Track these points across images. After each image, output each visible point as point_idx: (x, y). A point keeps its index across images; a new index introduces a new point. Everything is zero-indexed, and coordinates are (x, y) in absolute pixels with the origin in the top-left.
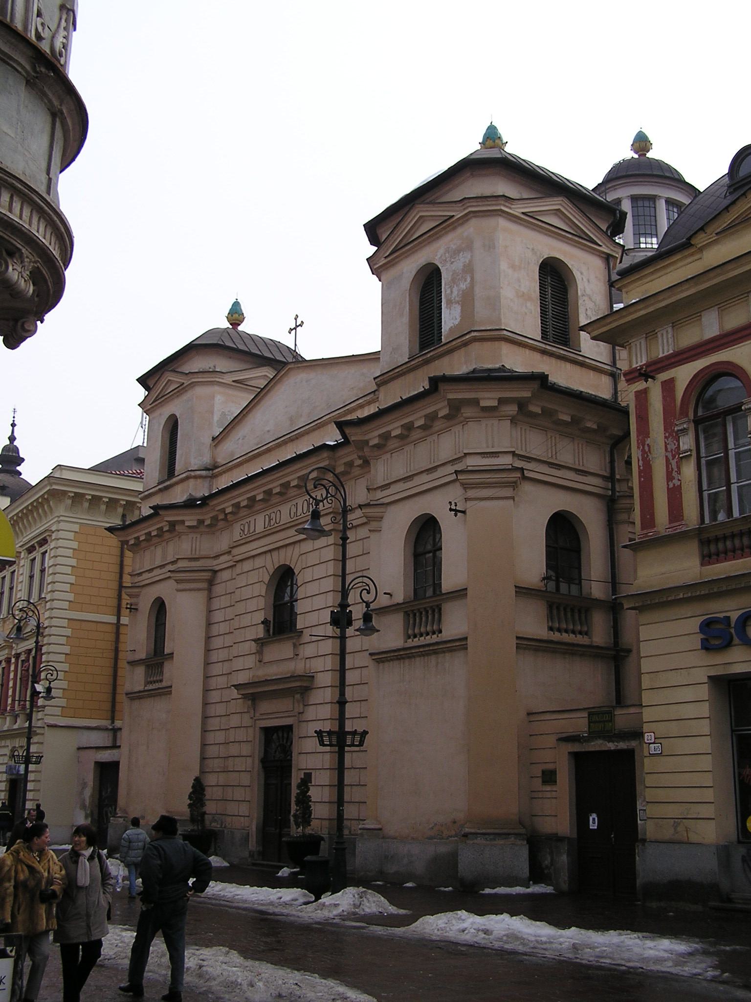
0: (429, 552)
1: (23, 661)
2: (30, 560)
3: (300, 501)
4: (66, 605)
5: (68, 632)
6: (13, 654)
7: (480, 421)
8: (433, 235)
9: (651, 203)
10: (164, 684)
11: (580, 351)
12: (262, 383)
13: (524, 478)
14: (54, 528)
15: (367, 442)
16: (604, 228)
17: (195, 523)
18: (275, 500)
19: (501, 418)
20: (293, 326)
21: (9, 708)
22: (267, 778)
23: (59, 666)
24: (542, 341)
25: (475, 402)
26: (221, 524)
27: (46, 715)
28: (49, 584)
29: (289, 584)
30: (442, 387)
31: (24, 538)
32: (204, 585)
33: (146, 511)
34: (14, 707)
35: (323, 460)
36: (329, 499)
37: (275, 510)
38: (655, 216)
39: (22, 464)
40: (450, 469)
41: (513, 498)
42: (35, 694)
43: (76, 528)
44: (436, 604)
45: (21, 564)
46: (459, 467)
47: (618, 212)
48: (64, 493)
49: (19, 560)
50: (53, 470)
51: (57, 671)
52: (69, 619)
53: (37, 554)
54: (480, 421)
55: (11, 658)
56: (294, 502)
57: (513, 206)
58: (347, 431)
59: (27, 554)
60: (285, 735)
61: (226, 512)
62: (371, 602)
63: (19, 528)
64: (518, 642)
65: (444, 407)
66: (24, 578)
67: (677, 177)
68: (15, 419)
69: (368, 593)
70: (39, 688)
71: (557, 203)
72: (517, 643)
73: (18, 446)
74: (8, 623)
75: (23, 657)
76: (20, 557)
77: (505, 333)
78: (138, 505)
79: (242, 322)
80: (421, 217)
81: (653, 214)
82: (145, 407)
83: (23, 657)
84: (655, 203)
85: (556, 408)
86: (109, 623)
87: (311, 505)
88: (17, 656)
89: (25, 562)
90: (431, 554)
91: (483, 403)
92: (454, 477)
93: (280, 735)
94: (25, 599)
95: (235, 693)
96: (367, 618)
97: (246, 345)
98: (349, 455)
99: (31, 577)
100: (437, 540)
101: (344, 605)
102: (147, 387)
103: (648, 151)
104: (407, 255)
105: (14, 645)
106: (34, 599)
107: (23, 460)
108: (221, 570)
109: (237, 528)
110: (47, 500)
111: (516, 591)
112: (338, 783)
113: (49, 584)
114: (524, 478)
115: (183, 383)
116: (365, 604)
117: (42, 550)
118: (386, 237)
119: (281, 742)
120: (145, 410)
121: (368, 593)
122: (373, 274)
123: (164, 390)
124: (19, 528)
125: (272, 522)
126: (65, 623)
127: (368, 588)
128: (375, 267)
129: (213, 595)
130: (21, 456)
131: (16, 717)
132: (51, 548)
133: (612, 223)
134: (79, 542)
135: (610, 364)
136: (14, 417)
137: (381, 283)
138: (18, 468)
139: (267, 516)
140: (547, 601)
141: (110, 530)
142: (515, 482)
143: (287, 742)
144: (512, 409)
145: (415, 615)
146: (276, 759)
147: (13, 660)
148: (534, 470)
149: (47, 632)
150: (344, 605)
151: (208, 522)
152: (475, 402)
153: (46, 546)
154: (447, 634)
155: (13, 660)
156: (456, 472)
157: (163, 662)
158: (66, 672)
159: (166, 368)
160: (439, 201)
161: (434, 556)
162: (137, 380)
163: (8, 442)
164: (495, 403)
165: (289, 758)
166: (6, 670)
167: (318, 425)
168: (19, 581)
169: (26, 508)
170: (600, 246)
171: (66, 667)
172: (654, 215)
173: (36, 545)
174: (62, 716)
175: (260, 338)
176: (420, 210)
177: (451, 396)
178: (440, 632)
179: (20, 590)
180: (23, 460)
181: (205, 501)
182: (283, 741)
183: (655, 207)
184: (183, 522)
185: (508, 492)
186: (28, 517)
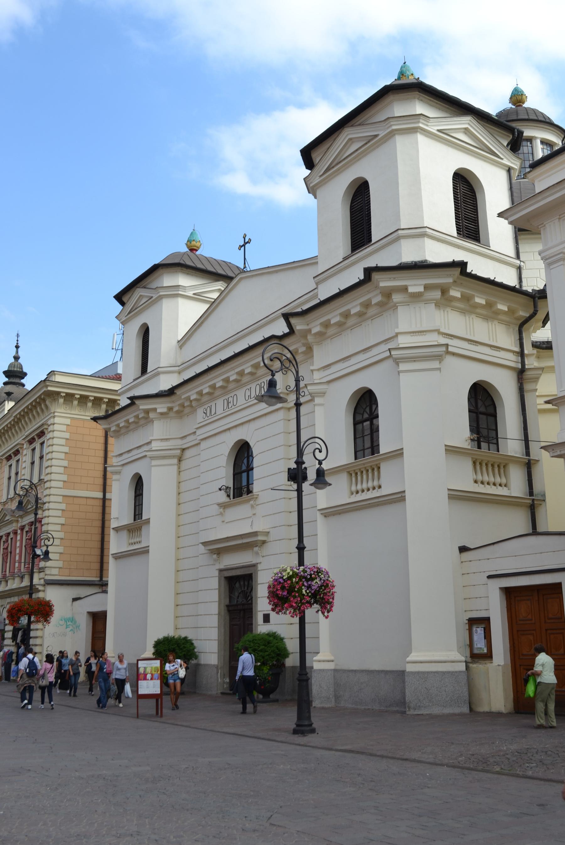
0: (366, 420)
1: (27, 532)
2: (32, 450)
3: (253, 386)
4: (60, 484)
5: (63, 506)
6: (19, 526)
7: (409, 305)
8: (358, 155)
9: (529, 143)
10: (143, 545)
11: (490, 247)
12: (215, 295)
13: (448, 352)
14: (49, 423)
15: (310, 331)
16: (505, 144)
17: (165, 410)
18: (231, 386)
19: (427, 302)
20: (242, 243)
21: (16, 571)
22: (231, 619)
23: (55, 535)
24: (458, 237)
25: (404, 289)
26: (187, 410)
27: (46, 575)
28: (47, 468)
29: (246, 455)
30: (376, 276)
31: (25, 432)
32: (175, 461)
33: (124, 402)
34: (20, 570)
35: (273, 349)
36: (283, 371)
37: (232, 394)
38: (533, 154)
39: (25, 378)
40: (384, 347)
41: (439, 369)
42: (35, 556)
43: (68, 422)
44: (375, 463)
45: (24, 453)
46: (391, 345)
47: (516, 130)
48: (58, 393)
49: (23, 450)
50: (47, 375)
51: (53, 538)
52: (63, 496)
53: (37, 445)
54: (409, 305)
55: (17, 530)
56: (248, 387)
57: (429, 124)
58: (293, 321)
59: (28, 445)
60: (246, 583)
61: (191, 399)
62: (323, 460)
63: (22, 424)
64: (449, 493)
65: (377, 295)
66: (28, 464)
67: (548, 121)
68: (18, 342)
69: (320, 451)
70: (38, 552)
71: (466, 122)
72: (448, 494)
73: (21, 363)
74: (14, 502)
75: (27, 529)
76: (23, 448)
77: (427, 230)
78: (118, 402)
79: (107, 604)
80: (350, 139)
81: (530, 152)
82: (121, 319)
83: (27, 529)
84: (531, 143)
85: (474, 293)
86: (97, 498)
87: (262, 389)
88: (22, 528)
89: (27, 451)
90: (368, 423)
91: (411, 290)
92: (387, 354)
93: (242, 583)
94: (28, 479)
95: (202, 549)
96: (320, 473)
97: (203, 264)
98: (293, 343)
99: (33, 463)
100: (373, 410)
101: (300, 462)
102: (123, 304)
103: (523, 103)
104: (339, 172)
105: (19, 519)
106: (35, 480)
107: (25, 374)
108: (188, 448)
109: (200, 413)
110: (44, 400)
111: (445, 449)
112: (524, 438)
113: (47, 468)
114: (448, 352)
115: (152, 297)
116: (318, 461)
117: (41, 440)
118: (319, 160)
119: (243, 589)
120: (121, 321)
121: (320, 451)
122: (309, 193)
123: (137, 304)
124: (22, 424)
125: (230, 405)
126: (60, 499)
127: (320, 448)
128: (311, 185)
129: (181, 470)
130: (25, 370)
131: (22, 578)
132: (48, 438)
133: (511, 141)
134: (64, 546)
135: (514, 257)
136: (17, 341)
137: (316, 200)
138: (23, 381)
139: (225, 401)
140: (472, 458)
141: (95, 419)
142: (441, 356)
143: (247, 589)
144: (437, 294)
145: (356, 474)
146: (239, 603)
147: (19, 532)
148: (456, 346)
149: (46, 507)
150: (300, 462)
151: (176, 409)
152: (404, 289)
153: (43, 437)
154: (385, 491)
155: (19, 532)
156: (389, 350)
157: (141, 527)
158: (61, 568)
159: (138, 285)
160: (366, 123)
161: (372, 424)
162: (115, 297)
163: (13, 360)
164: (421, 289)
165: (250, 602)
166: (14, 540)
167: (268, 320)
168: (22, 474)
169: (27, 407)
170: (502, 159)
171: (61, 535)
172: (531, 152)
173: (35, 437)
174: (59, 575)
175: (215, 259)
176: (347, 133)
177: (382, 284)
178: (380, 487)
179: (25, 461)
180: (25, 374)
181: (174, 391)
182: (244, 588)
183: (532, 147)
184: (155, 410)
185: (435, 364)
186: (28, 415)
